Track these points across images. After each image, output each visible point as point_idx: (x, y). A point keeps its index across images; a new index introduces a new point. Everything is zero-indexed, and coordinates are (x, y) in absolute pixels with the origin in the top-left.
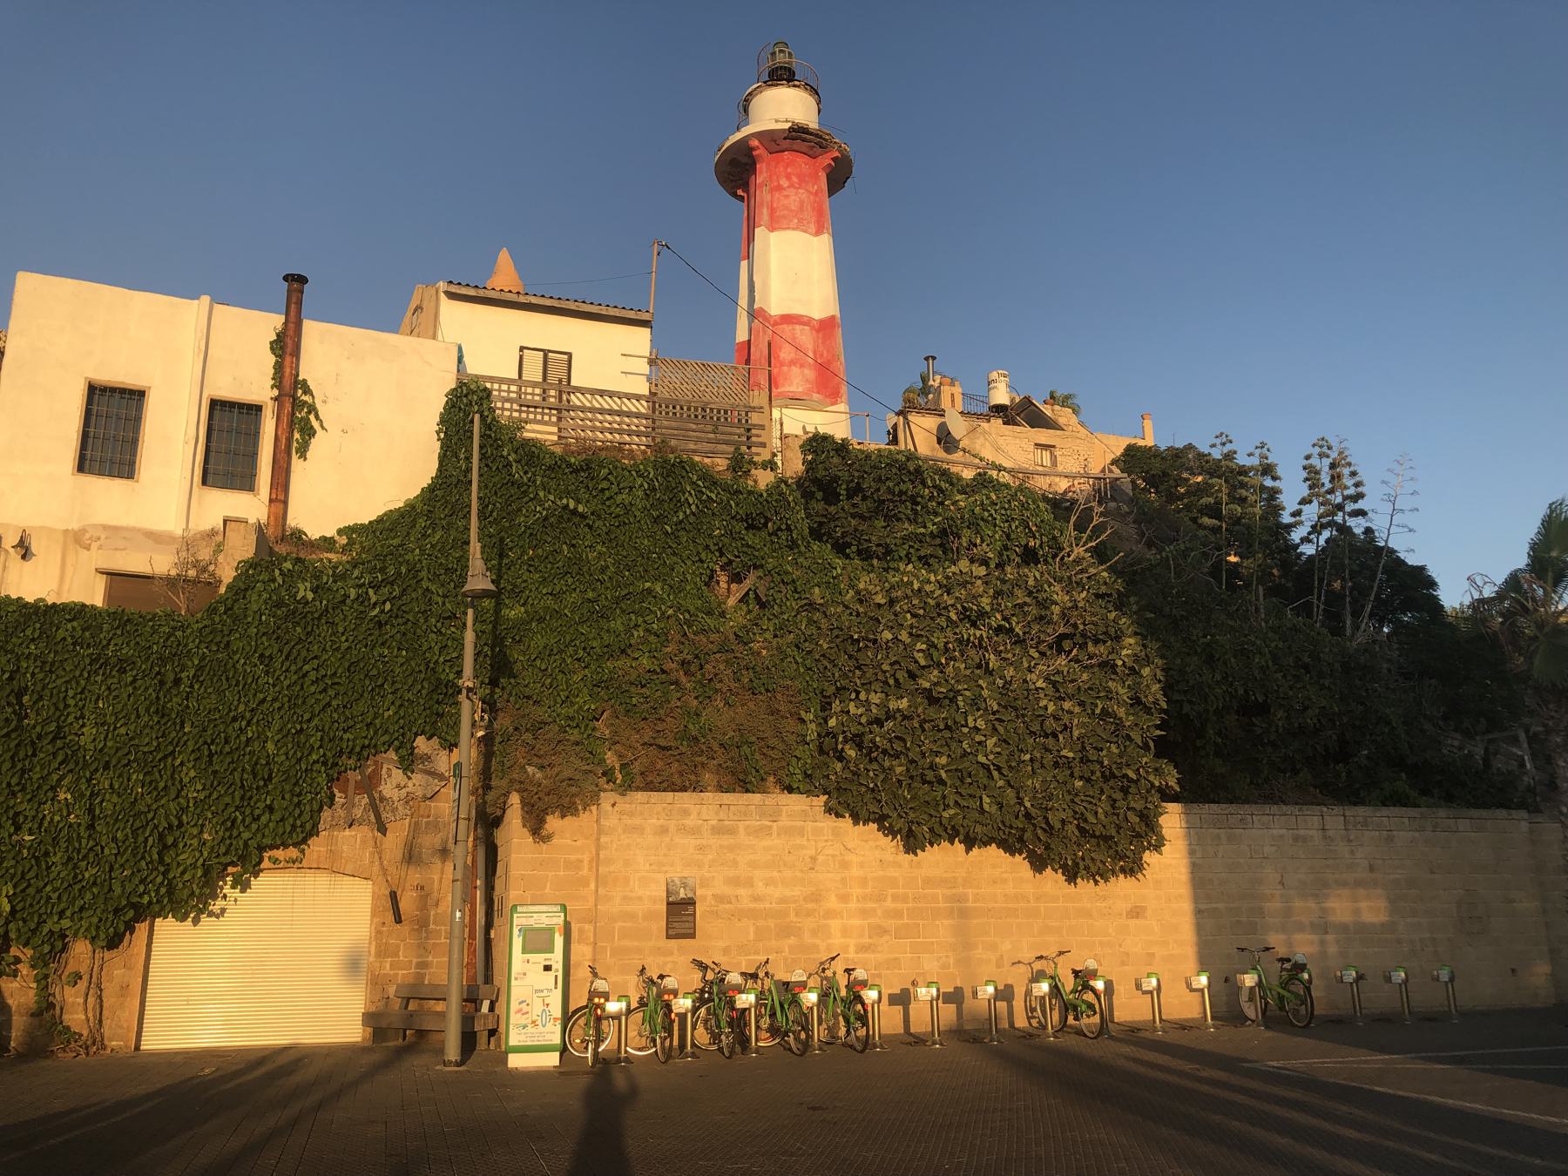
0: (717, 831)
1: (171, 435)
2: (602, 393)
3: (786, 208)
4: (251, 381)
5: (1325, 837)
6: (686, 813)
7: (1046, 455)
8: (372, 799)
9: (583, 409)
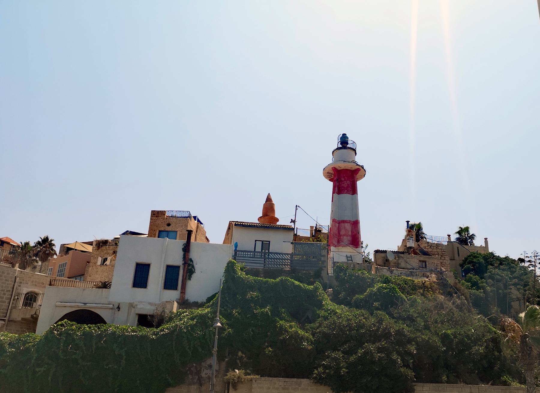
0: (283, 389)
1: (156, 276)
2: (277, 253)
3: (343, 187)
4: (177, 260)
8: (199, 377)
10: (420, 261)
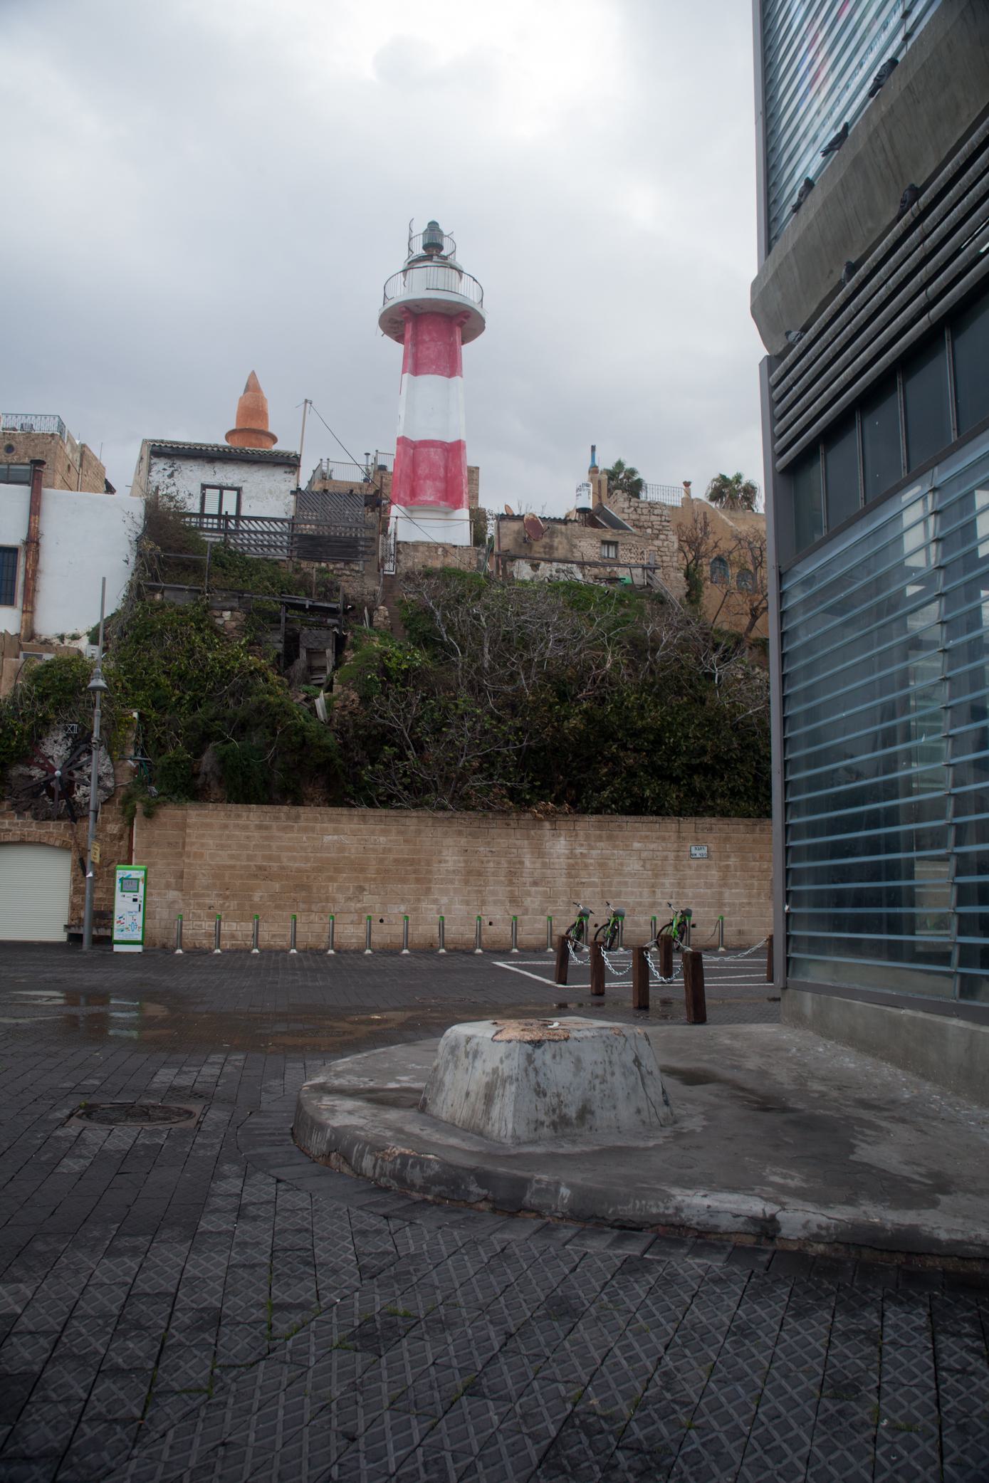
0: (260, 827)
5: (679, 837)
6: (239, 816)
7: (612, 550)
9: (249, 532)
10: (604, 542)
